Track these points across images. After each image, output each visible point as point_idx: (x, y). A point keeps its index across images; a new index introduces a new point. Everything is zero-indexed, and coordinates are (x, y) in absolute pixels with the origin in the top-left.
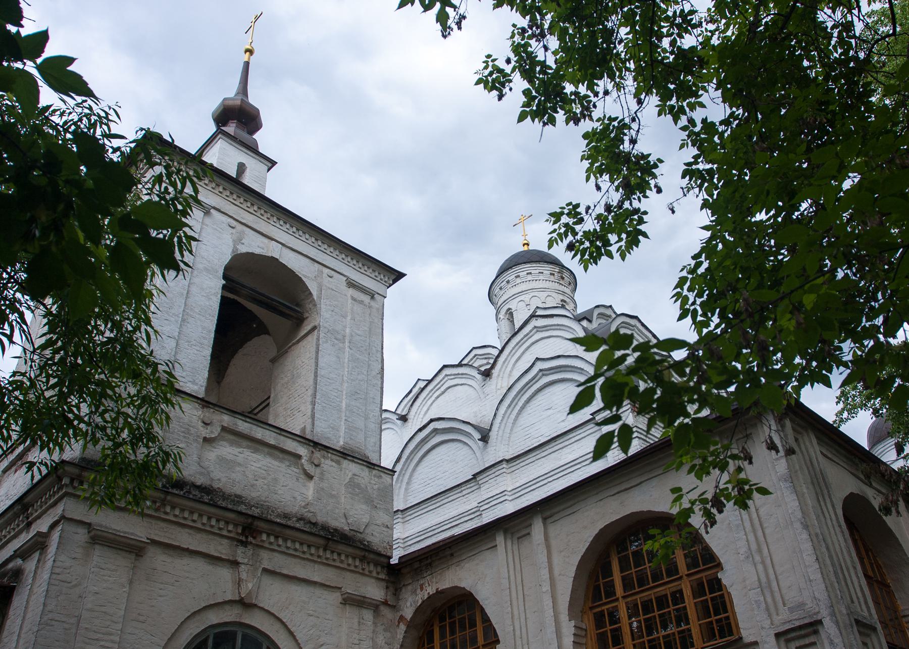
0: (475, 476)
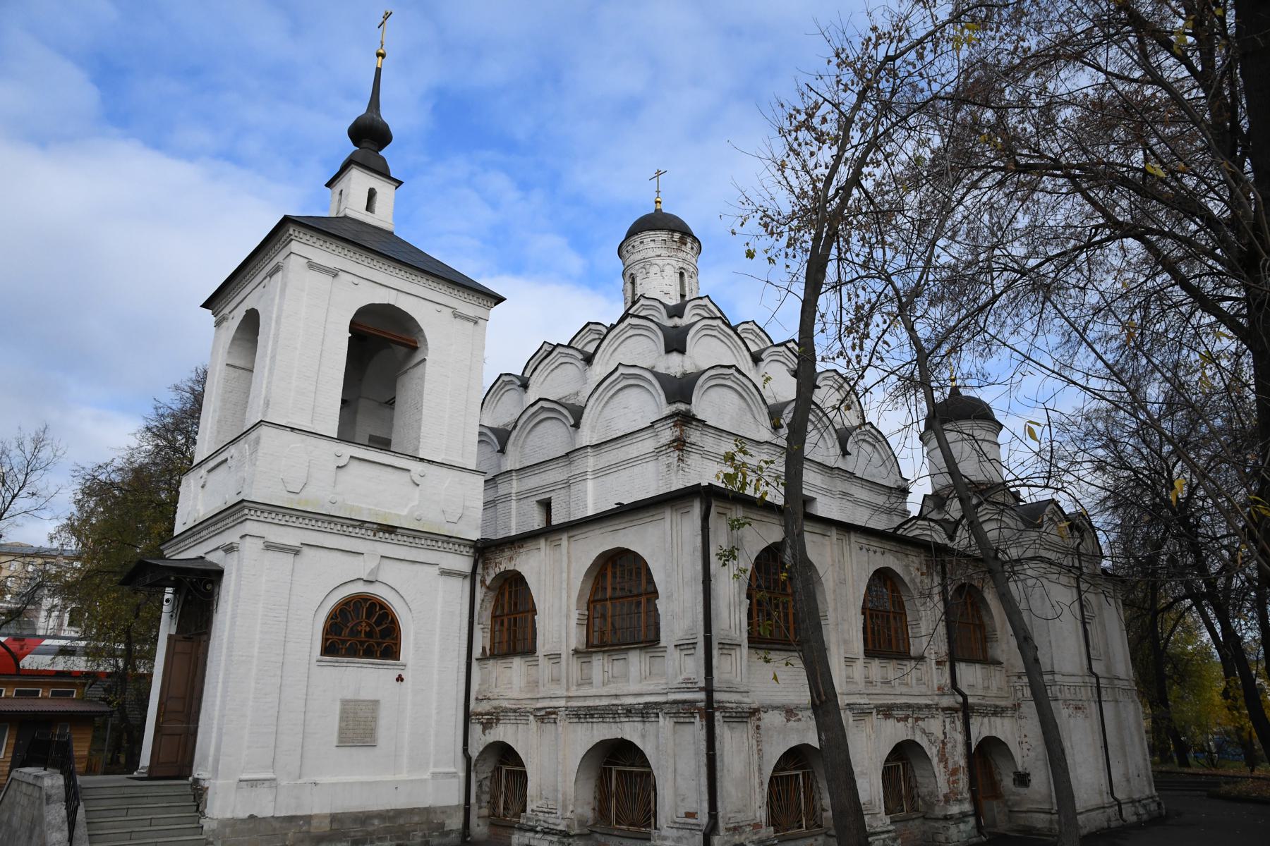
0: (567, 454)
